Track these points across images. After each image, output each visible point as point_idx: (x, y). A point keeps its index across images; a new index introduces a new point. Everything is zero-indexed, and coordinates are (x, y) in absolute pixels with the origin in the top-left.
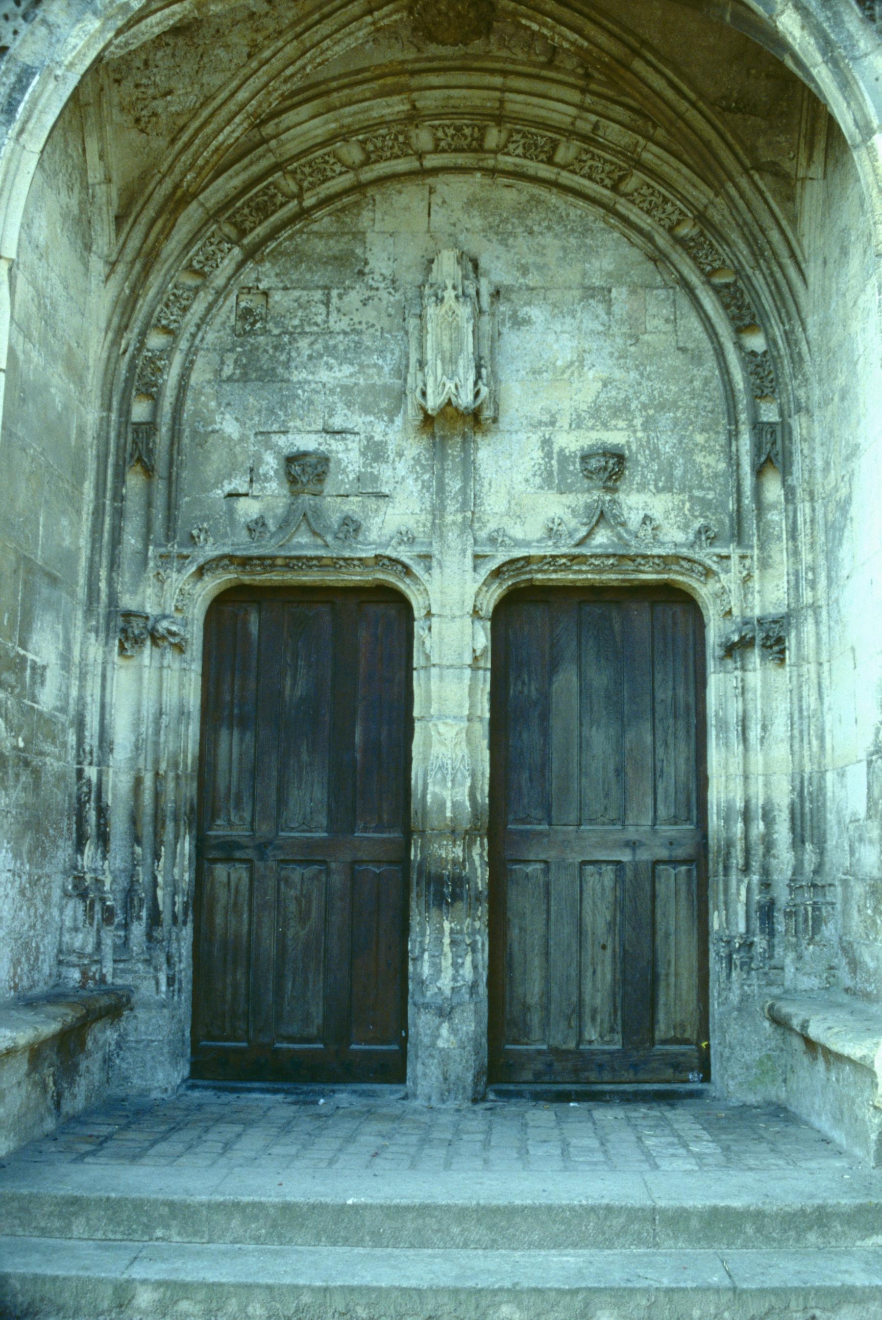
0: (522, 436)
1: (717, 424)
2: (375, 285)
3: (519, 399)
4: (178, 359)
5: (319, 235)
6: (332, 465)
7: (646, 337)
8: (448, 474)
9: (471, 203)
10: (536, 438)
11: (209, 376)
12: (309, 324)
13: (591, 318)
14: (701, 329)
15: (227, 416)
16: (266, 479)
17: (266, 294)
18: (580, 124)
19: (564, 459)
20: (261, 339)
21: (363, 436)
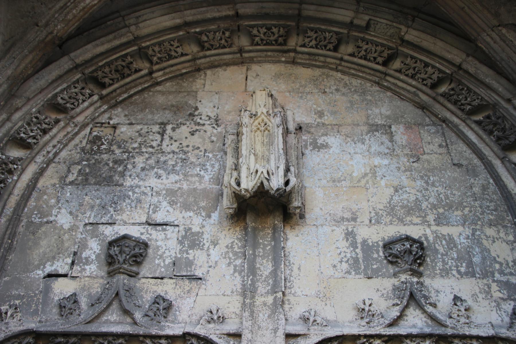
0: (327, 229)
1: (503, 219)
2: (201, 122)
3: (319, 199)
4: (31, 170)
5: (163, 93)
6: (150, 251)
7: (425, 157)
8: (259, 260)
9: (277, 76)
10: (339, 232)
11: (56, 181)
12: (146, 146)
13: (376, 143)
14: (469, 151)
15: (63, 211)
16: (87, 261)
17: (114, 127)
18: (356, 22)
19: (367, 248)
20: (105, 157)
21: (181, 228)
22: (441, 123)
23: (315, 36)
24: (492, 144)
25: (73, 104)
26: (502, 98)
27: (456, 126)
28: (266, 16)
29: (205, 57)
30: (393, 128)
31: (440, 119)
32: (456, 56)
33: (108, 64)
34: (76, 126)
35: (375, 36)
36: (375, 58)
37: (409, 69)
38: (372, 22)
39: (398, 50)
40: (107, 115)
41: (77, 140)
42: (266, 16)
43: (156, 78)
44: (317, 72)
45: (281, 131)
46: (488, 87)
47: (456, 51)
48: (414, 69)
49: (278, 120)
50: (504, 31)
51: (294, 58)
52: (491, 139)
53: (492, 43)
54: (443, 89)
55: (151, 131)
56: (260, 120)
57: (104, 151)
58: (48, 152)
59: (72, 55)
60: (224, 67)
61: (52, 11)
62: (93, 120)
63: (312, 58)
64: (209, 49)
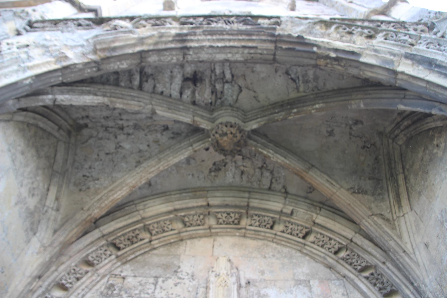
2: (182, 277)
5: (157, 255)
9: (234, 245)
12: (144, 293)
17: (124, 278)
18: (284, 210)
22: (342, 278)
23: (258, 219)
24: (377, 293)
25: (98, 261)
26: (380, 261)
27: (352, 280)
28: (227, 206)
29: (187, 231)
30: (312, 282)
31: (341, 275)
32: (349, 233)
33: (124, 235)
34: (99, 276)
35: (296, 220)
36: (297, 234)
37: (320, 241)
38: (294, 211)
39: (311, 229)
40: (119, 269)
41: (98, 286)
42: (227, 206)
43: (153, 245)
44: (260, 243)
45: (236, 287)
46: (370, 254)
47: (348, 230)
48: (323, 241)
49: (234, 279)
50: (375, 218)
51: (245, 233)
52: (376, 289)
53: (369, 226)
54: (343, 254)
55: (148, 282)
56: (221, 278)
57: (115, 295)
58: (79, 294)
59: (102, 228)
60: (199, 239)
61: (93, 201)
62: (110, 272)
63: (256, 233)
64: (189, 226)
